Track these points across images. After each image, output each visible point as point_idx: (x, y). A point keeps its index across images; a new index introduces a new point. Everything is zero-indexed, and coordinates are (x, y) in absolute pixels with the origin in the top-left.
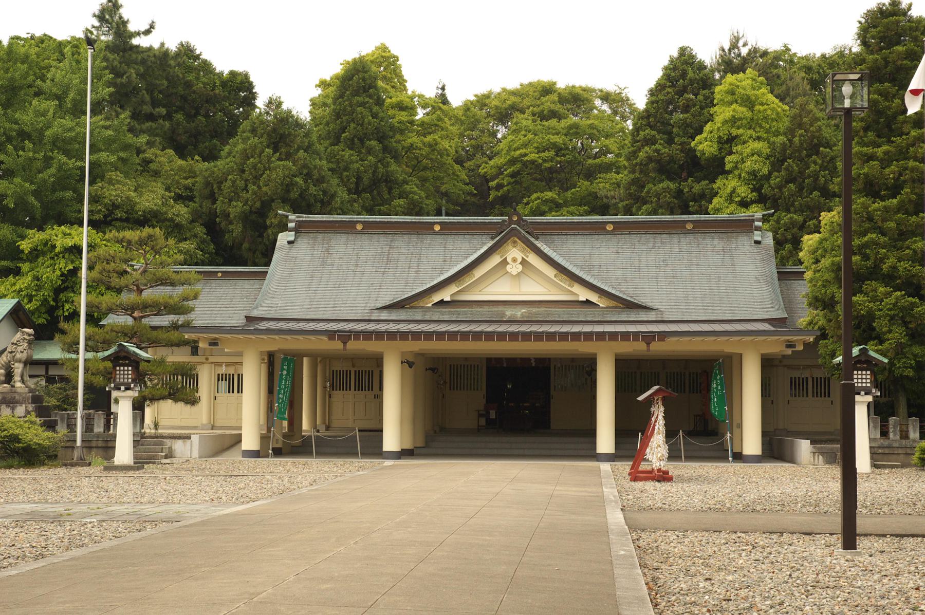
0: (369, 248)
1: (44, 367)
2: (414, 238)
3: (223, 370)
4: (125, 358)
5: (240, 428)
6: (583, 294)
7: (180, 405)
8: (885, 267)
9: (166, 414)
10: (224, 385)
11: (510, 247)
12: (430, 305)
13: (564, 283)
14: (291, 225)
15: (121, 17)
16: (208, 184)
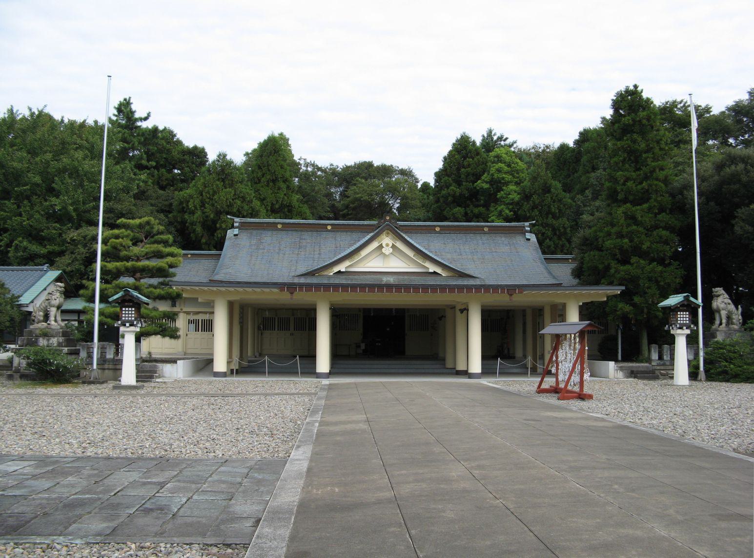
0: (287, 239)
1: (77, 315)
2: (315, 234)
3: (192, 317)
4: (130, 301)
5: (212, 354)
6: (432, 268)
7: (167, 339)
8: (644, 247)
9: (156, 345)
10: (192, 326)
11: (385, 236)
12: (332, 274)
13: (420, 261)
14: (236, 225)
15: (131, 109)
16: (181, 203)
